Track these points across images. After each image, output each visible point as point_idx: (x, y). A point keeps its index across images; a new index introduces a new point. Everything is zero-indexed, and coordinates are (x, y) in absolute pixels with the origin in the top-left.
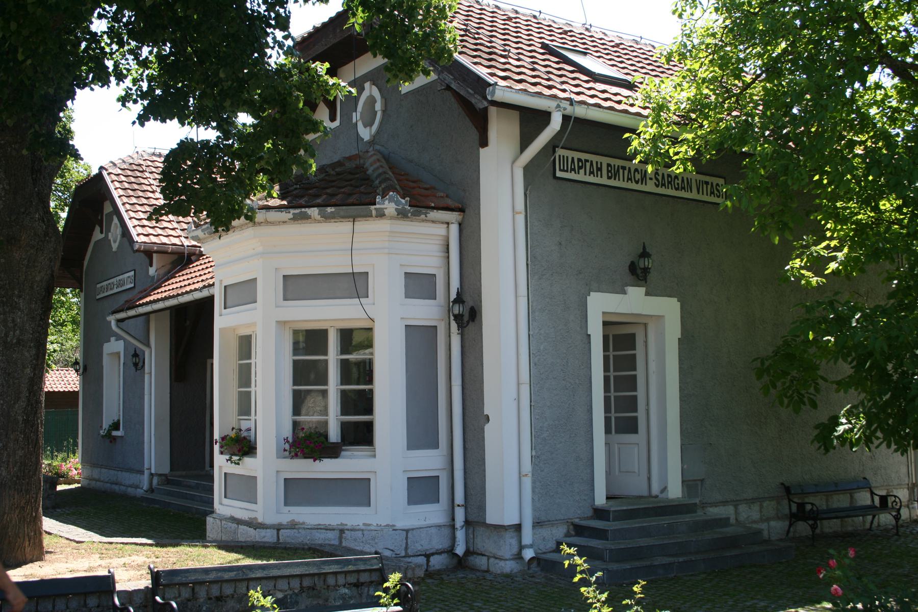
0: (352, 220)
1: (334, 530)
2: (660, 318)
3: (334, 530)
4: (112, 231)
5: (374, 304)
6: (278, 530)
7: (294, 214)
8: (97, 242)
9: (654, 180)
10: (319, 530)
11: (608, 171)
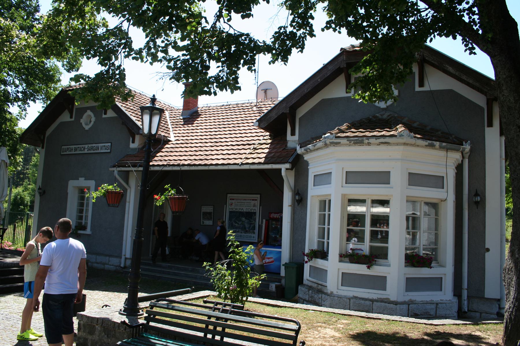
0: (446, 150)
1: (433, 304)
3: (433, 304)
4: (83, 118)
5: (342, 187)
6: (409, 305)
7: (429, 143)
8: (62, 124)
9: (87, 149)
10: (427, 304)
11: (75, 149)
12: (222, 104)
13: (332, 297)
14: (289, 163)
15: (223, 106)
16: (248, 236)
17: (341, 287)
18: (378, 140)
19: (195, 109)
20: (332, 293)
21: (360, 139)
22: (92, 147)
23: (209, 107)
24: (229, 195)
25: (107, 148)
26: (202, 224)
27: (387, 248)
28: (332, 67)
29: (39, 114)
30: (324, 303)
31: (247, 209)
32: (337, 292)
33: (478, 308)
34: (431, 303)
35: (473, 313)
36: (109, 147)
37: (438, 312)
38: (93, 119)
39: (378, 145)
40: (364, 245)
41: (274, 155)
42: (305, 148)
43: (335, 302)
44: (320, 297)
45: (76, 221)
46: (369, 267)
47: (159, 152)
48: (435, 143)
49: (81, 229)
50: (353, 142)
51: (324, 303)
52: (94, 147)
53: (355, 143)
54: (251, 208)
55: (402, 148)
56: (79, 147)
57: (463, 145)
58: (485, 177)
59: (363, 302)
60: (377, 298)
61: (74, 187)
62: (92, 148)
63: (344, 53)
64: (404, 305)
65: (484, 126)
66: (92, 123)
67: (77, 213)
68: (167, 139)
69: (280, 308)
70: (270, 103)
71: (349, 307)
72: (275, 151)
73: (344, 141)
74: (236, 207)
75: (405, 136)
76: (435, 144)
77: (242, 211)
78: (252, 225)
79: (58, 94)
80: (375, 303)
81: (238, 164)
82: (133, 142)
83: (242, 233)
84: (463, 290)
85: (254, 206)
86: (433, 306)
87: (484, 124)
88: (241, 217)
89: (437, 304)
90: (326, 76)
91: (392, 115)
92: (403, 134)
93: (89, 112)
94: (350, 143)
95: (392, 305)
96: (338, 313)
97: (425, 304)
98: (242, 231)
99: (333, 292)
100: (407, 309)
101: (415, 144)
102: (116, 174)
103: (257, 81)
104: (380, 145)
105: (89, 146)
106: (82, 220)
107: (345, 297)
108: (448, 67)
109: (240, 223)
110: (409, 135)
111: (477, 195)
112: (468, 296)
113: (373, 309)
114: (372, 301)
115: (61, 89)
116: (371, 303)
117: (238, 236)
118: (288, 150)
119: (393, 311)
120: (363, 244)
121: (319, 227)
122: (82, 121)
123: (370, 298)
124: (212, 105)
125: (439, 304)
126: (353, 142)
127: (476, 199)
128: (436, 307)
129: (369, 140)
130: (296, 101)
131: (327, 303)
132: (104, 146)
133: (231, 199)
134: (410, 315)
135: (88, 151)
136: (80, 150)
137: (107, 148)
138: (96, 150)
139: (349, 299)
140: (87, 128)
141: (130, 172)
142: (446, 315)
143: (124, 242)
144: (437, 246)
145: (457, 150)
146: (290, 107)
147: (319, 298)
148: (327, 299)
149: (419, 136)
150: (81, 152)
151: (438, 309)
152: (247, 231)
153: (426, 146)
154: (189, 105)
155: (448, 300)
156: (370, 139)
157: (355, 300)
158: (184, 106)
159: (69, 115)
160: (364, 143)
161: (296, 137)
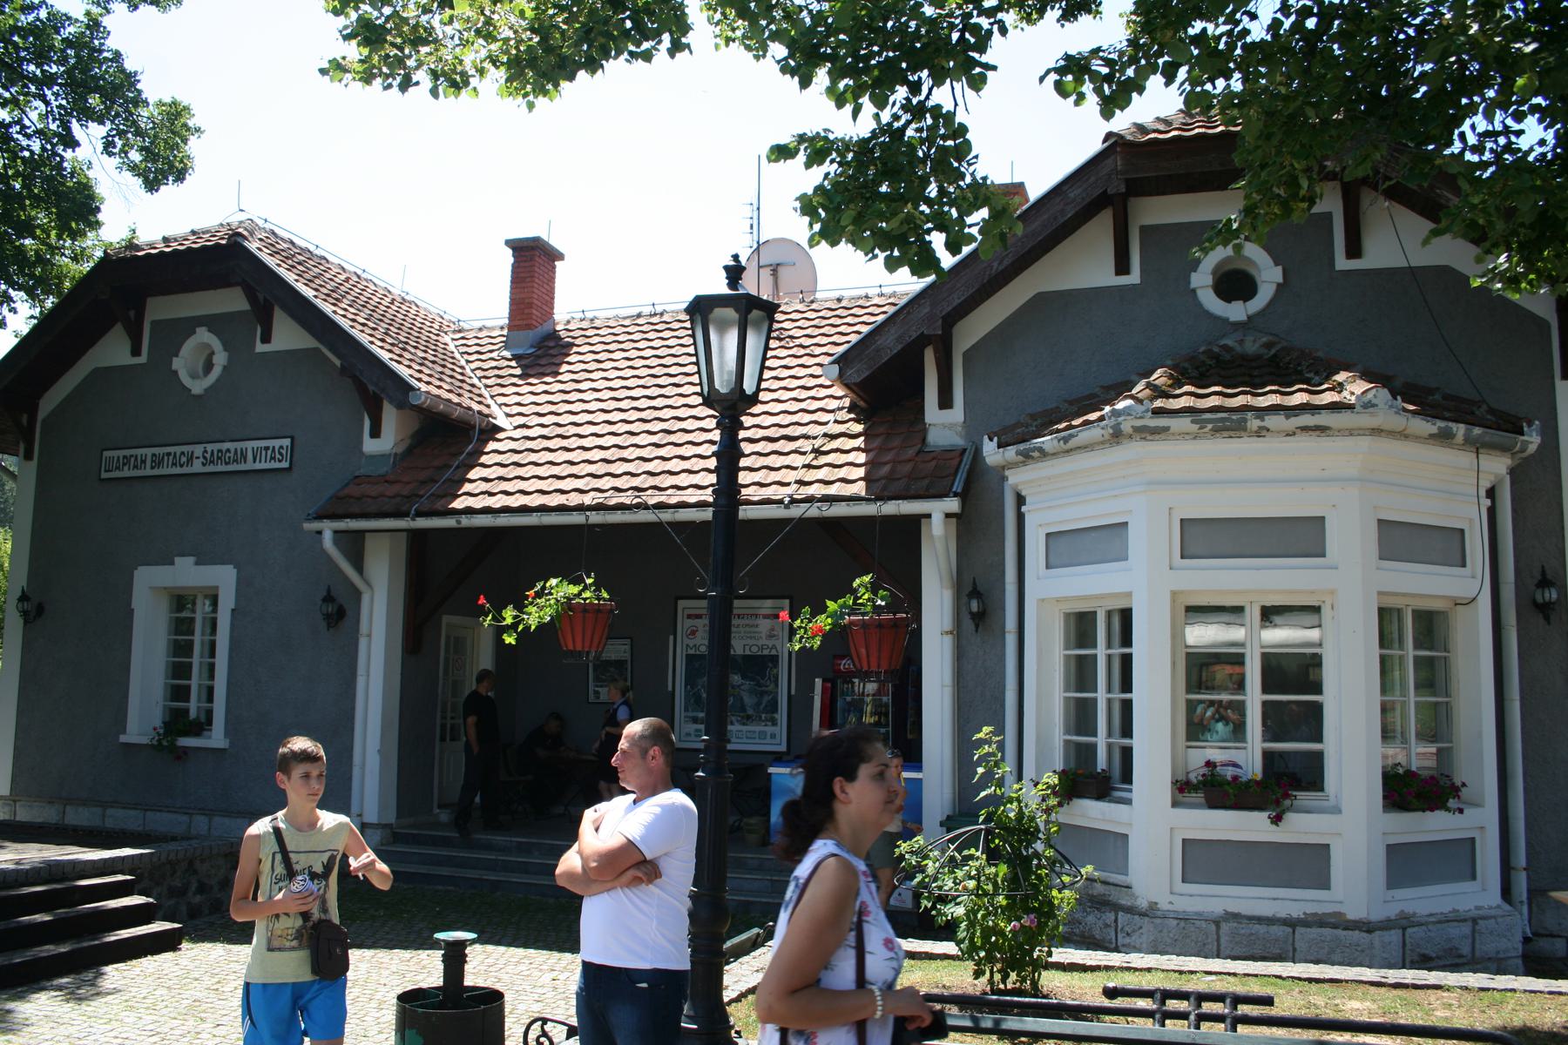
1: (1465, 920)
2: (929, 516)
3: (1465, 920)
6: (1404, 929)
7: (1439, 428)
8: (100, 374)
9: (202, 459)
10: (1450, 924)
11: (152, 461)
12: (635, 311)
13: (1158, 921)
14: (956, 495)
15: (639, 316)
16: (754, 732)
17: (1181, 887)
18: (1293, 419)
19: (546, 328)
20: (1153, 906)
21: (1234, 417)
23: (592, 320)
24: (682, 604)
25: (278, 456)
26: (592, 698)
27: (1319, 757)
28: (1080, 190)
29: (17, 340)
30: (1127, 940)
31: (747, 647)
32: (1171, 903)
33: (1560, 924)
34: (1455, 918)
35: (1545, 939)
36: (284, 452)
37: (1477, 946)
38: (220, 359)
39: (1288, 435)
40: (1245, 748)
41: (892, 471)
42: (1022, 447)
43: (1171, 935)
44: (1108, 922)
45: (164, 706)
46: (1276, 820)
47: (473, 467)
48: (1453, 425)
49: (186, 734)
50: (1210, 426)
51: (1127, 940)
52: (228, 450)
53: (1216, 430)
54: (760, 643)
55: (1365, 442)
56: (169, 454)
57: (1522, 434)
58: (1563, 528)
59: (1261, 929)
60: (1305, 913)
62: (220, 457)
63: (1118, 149)
64: (1393, 932)
65: (1553, 377)
66: (216, 371)
67: (167, 678)
68: (489, 422)
69: (1088, 975)
70: (801, 307)
71: (1215, 948)
72: (889, 456)
73: (1184, 423)
75: (1381, 405)
76: (1455, 429)
78: (766, 699)
79: (89, 272)
80: (1300, 930)
81: (780, 502)
82: (375, 433)
84: (1512, 872)
85: (771, 636)
86: (1466, 929)
87: (1553, 369)
89: (1474, 921)
90: (1062, 220)
91: (1285, 344)
92: (1374, 401)
93: (203, 335)
94: (1200, 428)
95: (1357, 932)
96: (1292, 977)
97: (1446, 925)
99: (1156, 903)
100: (1401, 945)
101: (1404, 430)
102: (328, 537)
103: (756, 239)
104: (1294, 434)
105: (209, 450)
106: (188, 700)
107: (1200, 916)
108: (1450, 196)
110: (1390, 403)
111: (1544, 583)
112: (1529, 891)
113: (1295, 950)
114: (1291, 923)
115: (99, 254)
116: (1290, 930)
118: (932, 454)
119: (1363, 951)
120: (1244, 745)
121: (1066, 699)
122: (177, 364)
123: (1278, 915)
124: (602, 314)
125: (1480, 922)
126: (1210, 426)
127: (1547, 595)
128: (1474, 931)
129: (1263, 420)
130: (963, 298)
131: (1144, 939)
132: (267, 448)
133: (689, 616)
134: (1407, 961)
135: (204, 464)
136: (174, 464)
137: (278, 456)
138: (235, 461)
139: (1214, 922)
140: (198, 387)
141: (367, 535)
142: (1498, 952)
143: (356, 771)
144: (1451, 742)
145: (1503, 449)
146: (943, 317)
147: (1107, 926)
148: (1141, 928)
149: (1411, 407)
150: (178, 470)
151: (1477, 935)
152: (749, 717)
153: (1432, 436)
154: (532, 314)
155: (1494, 905)
156: (1266, 418)
157: (1235, 924)
158: (512, 316)
160: (1245, 430)
161: (957, 414)
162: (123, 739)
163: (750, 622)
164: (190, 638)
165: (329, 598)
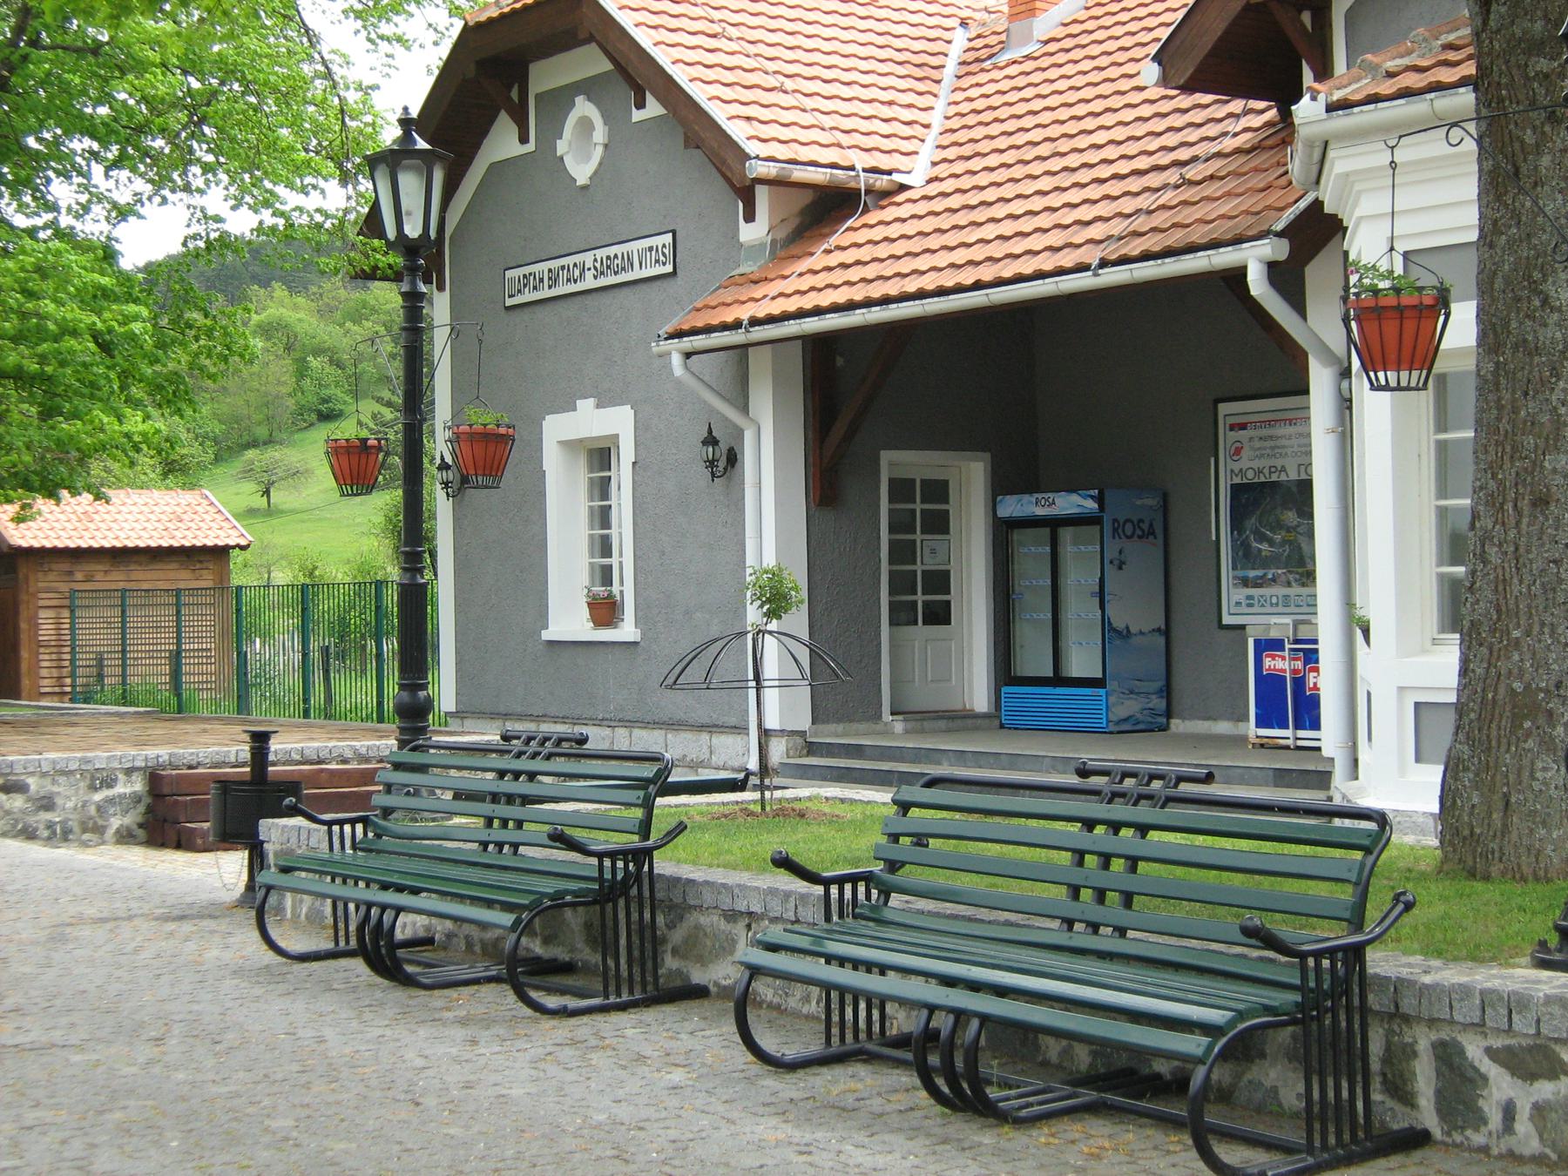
8: (495, 168)
9: (593, 271)
11: (550, 279)
22: (608, 258)
24: (1224, 408)
36: (666, 251)
38: (600, 134)
61: (569, 446)
74: (1256, 464)
77: (1283, 477)
82: (750, 217)
83: (1289, 584)
88: (1278, 511)
93: (584, 107)
98: (1291, 577)
109: (1278, 538)
117: (1274, 600)
132: (651, 249)
133: (1232, 428)
135: (595, 277)
137: (662, 258)
150: (572, 288)
159: (513, 131)
162: (546, 635)
163: (1265, 432)
164: (918, 529)
165: (710, 440)
